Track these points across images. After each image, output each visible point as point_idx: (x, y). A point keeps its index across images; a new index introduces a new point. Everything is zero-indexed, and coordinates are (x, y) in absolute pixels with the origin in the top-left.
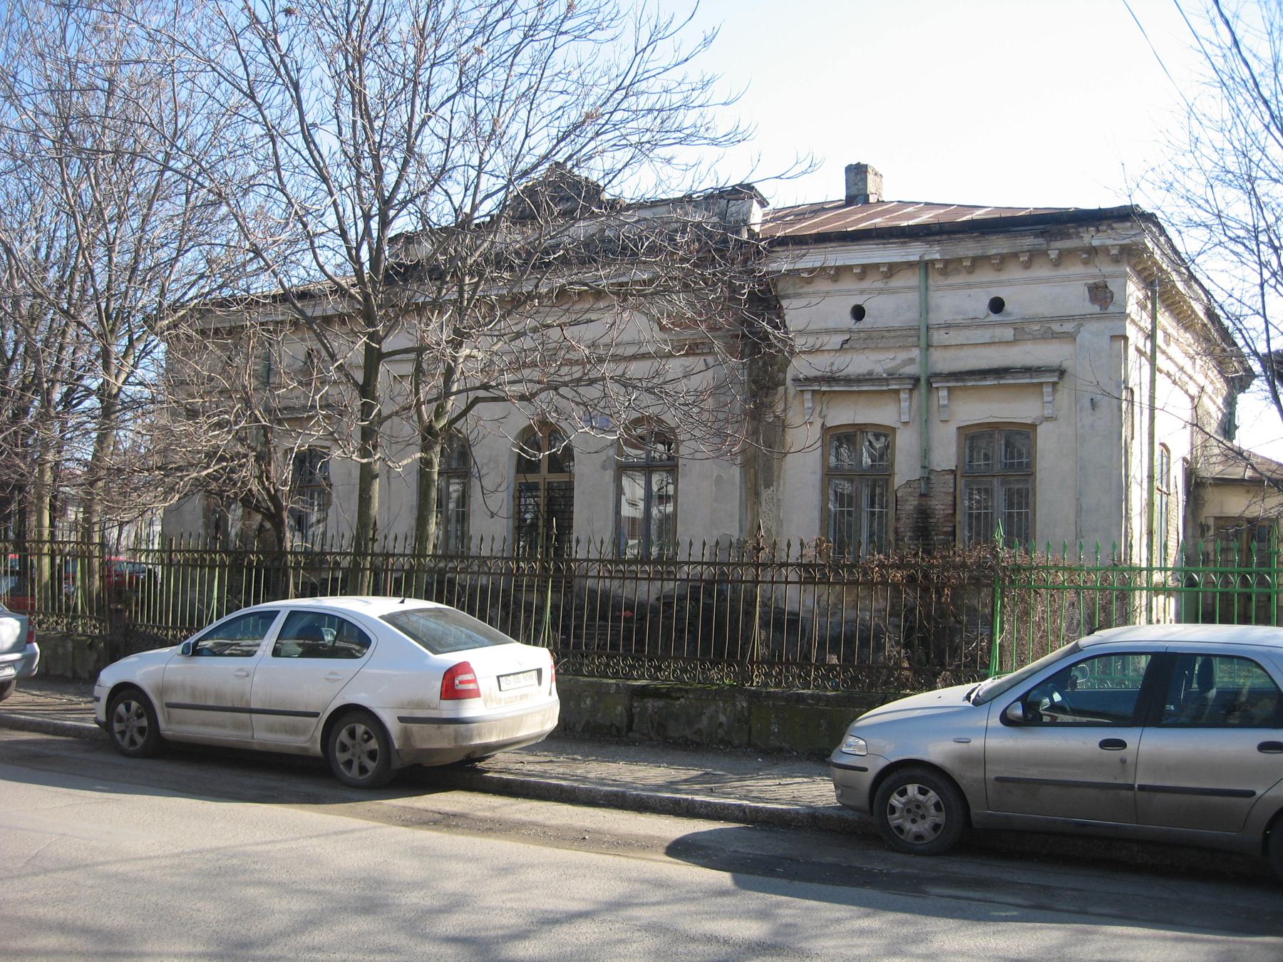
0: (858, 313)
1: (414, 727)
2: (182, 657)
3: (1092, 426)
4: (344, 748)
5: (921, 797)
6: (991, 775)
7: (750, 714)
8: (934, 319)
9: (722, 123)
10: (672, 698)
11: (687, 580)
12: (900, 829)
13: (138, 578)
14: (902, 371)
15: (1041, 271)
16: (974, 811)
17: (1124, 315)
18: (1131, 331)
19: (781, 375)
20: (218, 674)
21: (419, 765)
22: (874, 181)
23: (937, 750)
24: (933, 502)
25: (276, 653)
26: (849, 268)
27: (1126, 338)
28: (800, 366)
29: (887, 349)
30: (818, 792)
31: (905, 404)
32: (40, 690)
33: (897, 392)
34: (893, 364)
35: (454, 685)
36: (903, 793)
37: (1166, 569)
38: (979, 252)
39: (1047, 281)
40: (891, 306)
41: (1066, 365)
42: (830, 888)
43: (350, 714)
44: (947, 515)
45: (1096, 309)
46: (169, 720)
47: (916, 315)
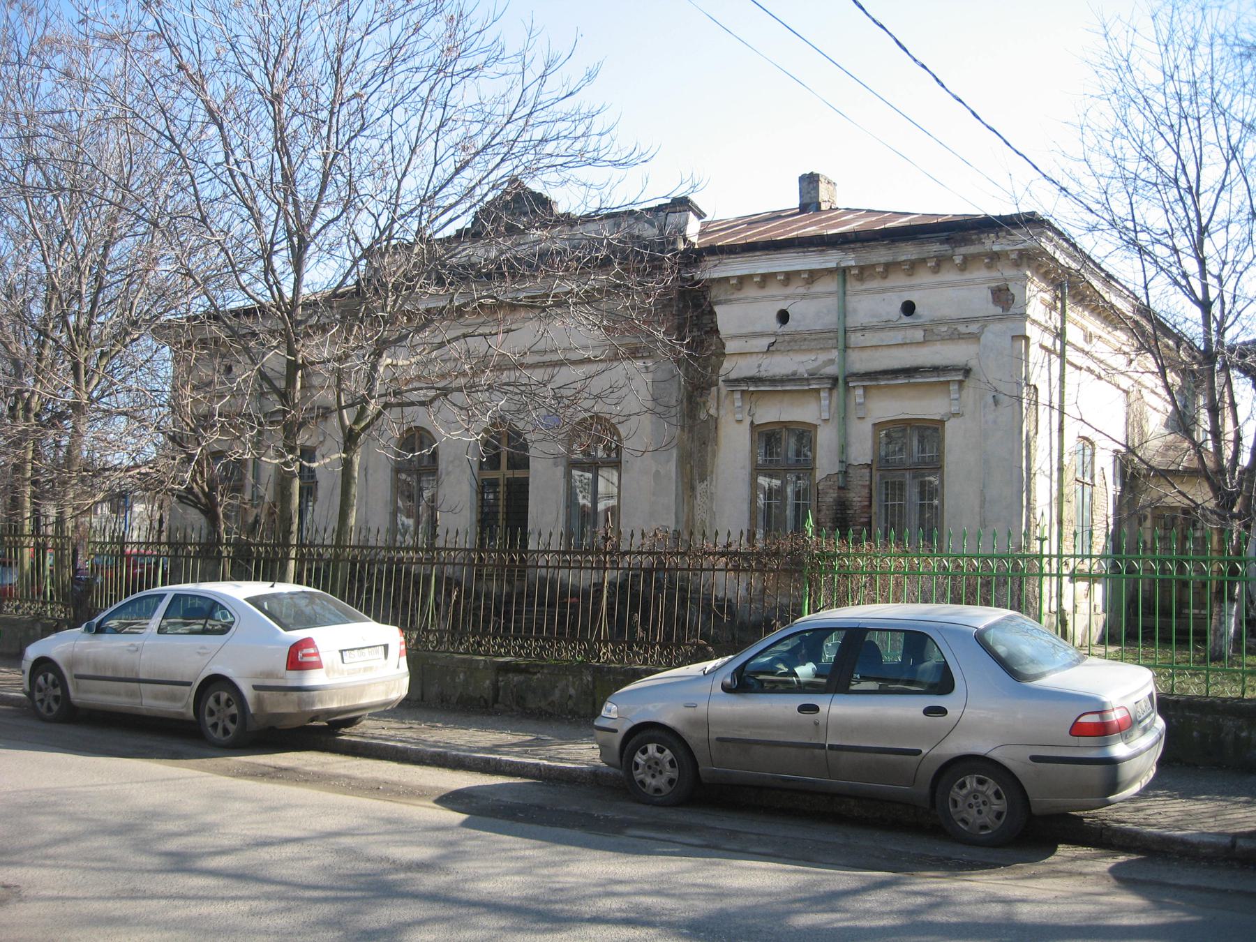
0: (783, 317)
1: (266, 694)
2: (87, 635)
3: (995, 422)
4: (212, 713)
5: (658, 755)
6: (713, 736)
7: (594, 687)
8: (852, 322)
9: (621, 145)
10: (530, 673)
11: (630, 569)
12: (642, 782)
13: (408, 573)
14: (823, 371)
15: (948, 275)
16: (702, 768)
17: (1024, 316)
18: (1031, 331)
19: (714, 378)
20: (109, 648)
21: (272, 728)
22: (827, 190)
23: (668, 713)
24: (852, 495)
25: (161, 631)
26: (773, 275)
27: (1027, 339)
28: (733, 367)
29: (810, 350)
30: (583, 754)
31: (825, 403)
32: (9, 667)
33: (818, 391)
34: (815, 364)
35: (298, 658)
36: (645, 752)
37: (1091, 557)
38: (890, 259)
39: (953, 284)
40: (812, 310)
41: (973, 363)
42: (540, 828)
43: (215, 682)
44: (864, 507)
45: (999, 310)
46: (77, 689)
47: (835, 319)
